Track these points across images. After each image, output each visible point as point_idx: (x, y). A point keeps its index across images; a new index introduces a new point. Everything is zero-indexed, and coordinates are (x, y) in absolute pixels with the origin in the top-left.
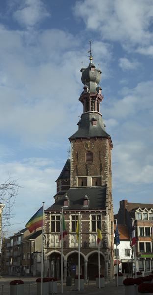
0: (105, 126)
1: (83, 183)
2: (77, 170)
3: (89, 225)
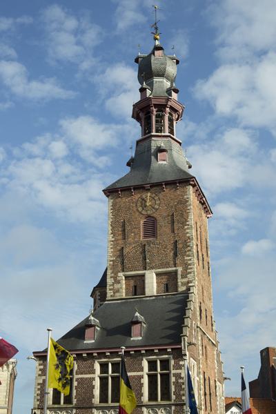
0: (190, 167)
1: (135, 287)
2: (123, 260)
3: (142, 385)
